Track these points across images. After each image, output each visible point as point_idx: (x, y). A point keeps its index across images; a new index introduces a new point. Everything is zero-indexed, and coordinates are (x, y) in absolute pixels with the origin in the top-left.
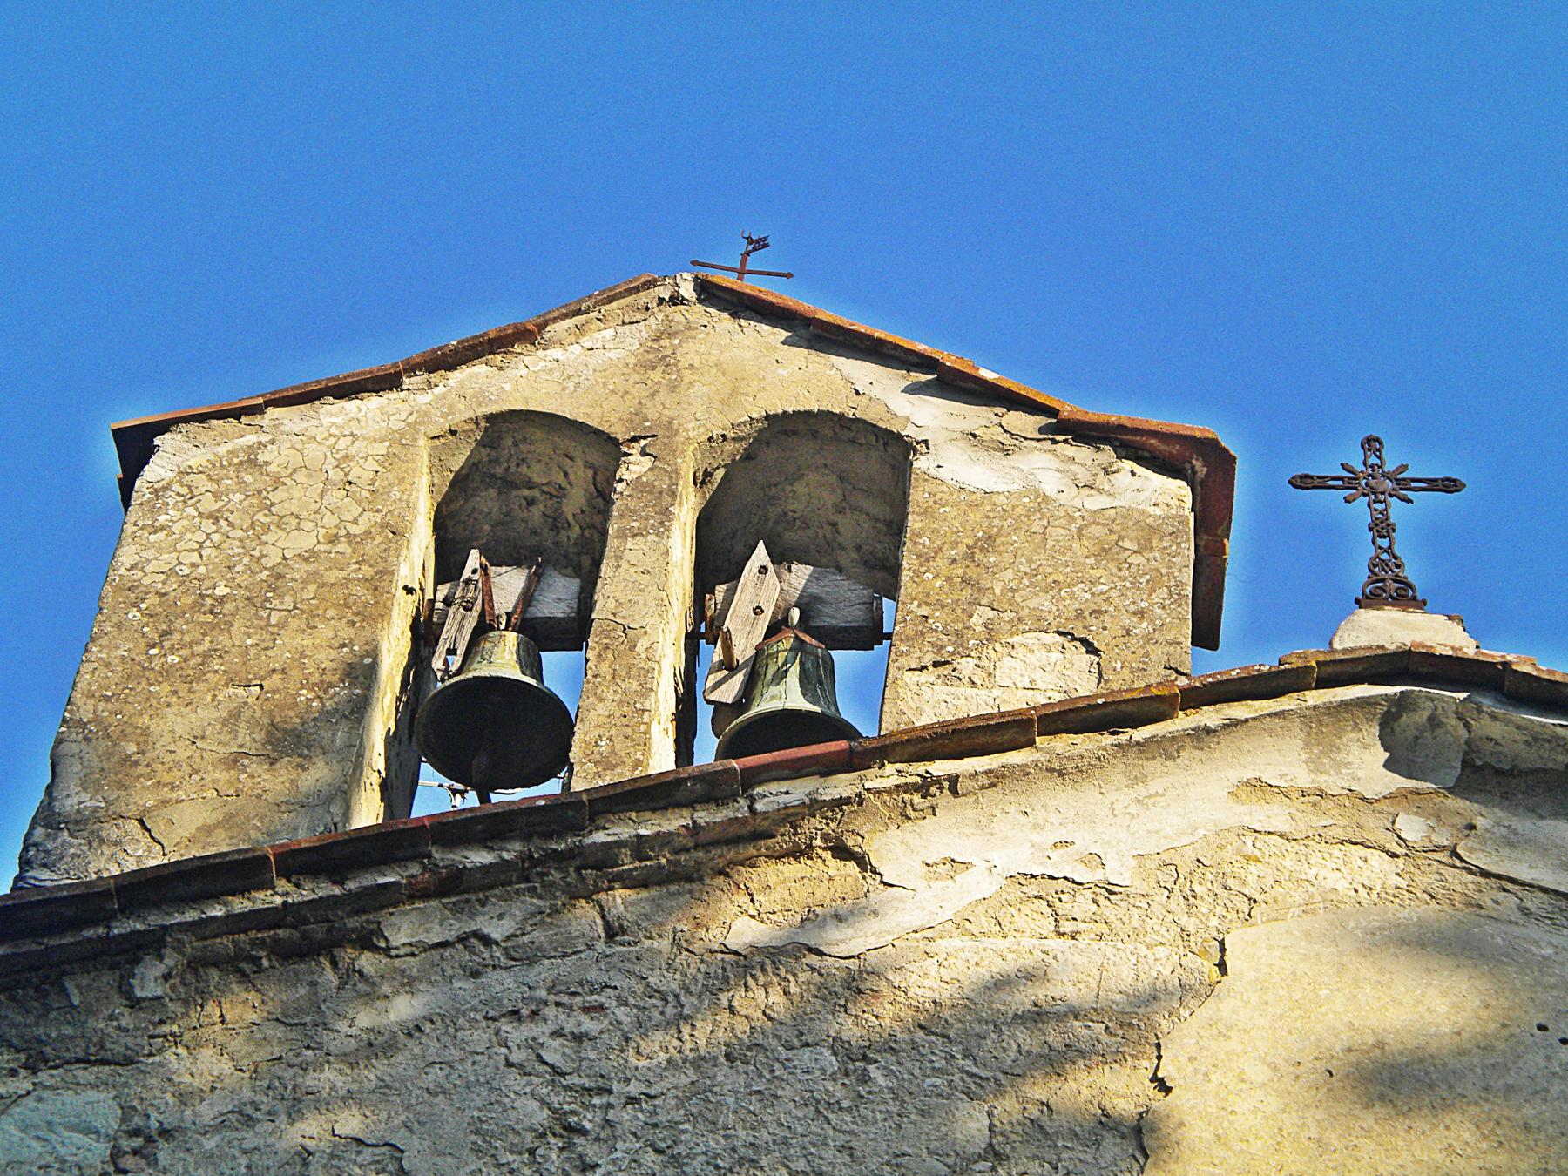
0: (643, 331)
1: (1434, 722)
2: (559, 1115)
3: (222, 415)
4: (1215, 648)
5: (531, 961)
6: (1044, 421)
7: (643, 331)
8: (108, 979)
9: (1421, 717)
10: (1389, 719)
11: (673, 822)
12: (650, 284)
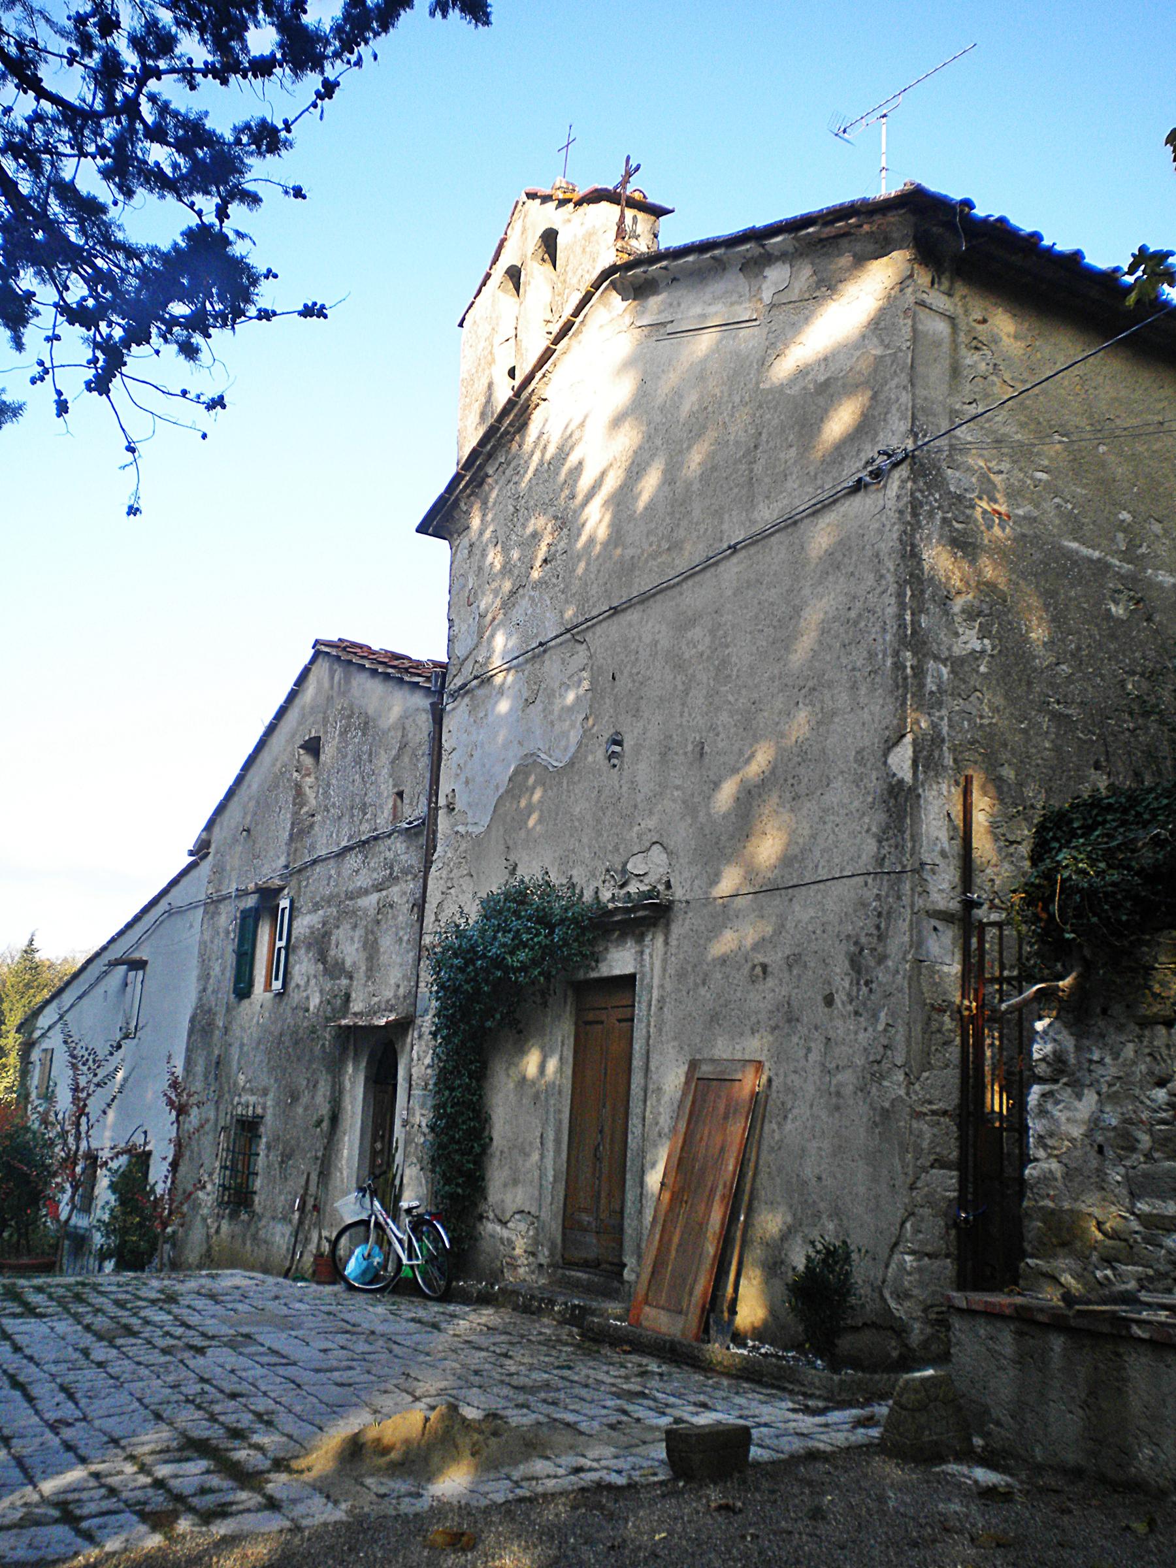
6: (571, 205)
10: (613, 285)
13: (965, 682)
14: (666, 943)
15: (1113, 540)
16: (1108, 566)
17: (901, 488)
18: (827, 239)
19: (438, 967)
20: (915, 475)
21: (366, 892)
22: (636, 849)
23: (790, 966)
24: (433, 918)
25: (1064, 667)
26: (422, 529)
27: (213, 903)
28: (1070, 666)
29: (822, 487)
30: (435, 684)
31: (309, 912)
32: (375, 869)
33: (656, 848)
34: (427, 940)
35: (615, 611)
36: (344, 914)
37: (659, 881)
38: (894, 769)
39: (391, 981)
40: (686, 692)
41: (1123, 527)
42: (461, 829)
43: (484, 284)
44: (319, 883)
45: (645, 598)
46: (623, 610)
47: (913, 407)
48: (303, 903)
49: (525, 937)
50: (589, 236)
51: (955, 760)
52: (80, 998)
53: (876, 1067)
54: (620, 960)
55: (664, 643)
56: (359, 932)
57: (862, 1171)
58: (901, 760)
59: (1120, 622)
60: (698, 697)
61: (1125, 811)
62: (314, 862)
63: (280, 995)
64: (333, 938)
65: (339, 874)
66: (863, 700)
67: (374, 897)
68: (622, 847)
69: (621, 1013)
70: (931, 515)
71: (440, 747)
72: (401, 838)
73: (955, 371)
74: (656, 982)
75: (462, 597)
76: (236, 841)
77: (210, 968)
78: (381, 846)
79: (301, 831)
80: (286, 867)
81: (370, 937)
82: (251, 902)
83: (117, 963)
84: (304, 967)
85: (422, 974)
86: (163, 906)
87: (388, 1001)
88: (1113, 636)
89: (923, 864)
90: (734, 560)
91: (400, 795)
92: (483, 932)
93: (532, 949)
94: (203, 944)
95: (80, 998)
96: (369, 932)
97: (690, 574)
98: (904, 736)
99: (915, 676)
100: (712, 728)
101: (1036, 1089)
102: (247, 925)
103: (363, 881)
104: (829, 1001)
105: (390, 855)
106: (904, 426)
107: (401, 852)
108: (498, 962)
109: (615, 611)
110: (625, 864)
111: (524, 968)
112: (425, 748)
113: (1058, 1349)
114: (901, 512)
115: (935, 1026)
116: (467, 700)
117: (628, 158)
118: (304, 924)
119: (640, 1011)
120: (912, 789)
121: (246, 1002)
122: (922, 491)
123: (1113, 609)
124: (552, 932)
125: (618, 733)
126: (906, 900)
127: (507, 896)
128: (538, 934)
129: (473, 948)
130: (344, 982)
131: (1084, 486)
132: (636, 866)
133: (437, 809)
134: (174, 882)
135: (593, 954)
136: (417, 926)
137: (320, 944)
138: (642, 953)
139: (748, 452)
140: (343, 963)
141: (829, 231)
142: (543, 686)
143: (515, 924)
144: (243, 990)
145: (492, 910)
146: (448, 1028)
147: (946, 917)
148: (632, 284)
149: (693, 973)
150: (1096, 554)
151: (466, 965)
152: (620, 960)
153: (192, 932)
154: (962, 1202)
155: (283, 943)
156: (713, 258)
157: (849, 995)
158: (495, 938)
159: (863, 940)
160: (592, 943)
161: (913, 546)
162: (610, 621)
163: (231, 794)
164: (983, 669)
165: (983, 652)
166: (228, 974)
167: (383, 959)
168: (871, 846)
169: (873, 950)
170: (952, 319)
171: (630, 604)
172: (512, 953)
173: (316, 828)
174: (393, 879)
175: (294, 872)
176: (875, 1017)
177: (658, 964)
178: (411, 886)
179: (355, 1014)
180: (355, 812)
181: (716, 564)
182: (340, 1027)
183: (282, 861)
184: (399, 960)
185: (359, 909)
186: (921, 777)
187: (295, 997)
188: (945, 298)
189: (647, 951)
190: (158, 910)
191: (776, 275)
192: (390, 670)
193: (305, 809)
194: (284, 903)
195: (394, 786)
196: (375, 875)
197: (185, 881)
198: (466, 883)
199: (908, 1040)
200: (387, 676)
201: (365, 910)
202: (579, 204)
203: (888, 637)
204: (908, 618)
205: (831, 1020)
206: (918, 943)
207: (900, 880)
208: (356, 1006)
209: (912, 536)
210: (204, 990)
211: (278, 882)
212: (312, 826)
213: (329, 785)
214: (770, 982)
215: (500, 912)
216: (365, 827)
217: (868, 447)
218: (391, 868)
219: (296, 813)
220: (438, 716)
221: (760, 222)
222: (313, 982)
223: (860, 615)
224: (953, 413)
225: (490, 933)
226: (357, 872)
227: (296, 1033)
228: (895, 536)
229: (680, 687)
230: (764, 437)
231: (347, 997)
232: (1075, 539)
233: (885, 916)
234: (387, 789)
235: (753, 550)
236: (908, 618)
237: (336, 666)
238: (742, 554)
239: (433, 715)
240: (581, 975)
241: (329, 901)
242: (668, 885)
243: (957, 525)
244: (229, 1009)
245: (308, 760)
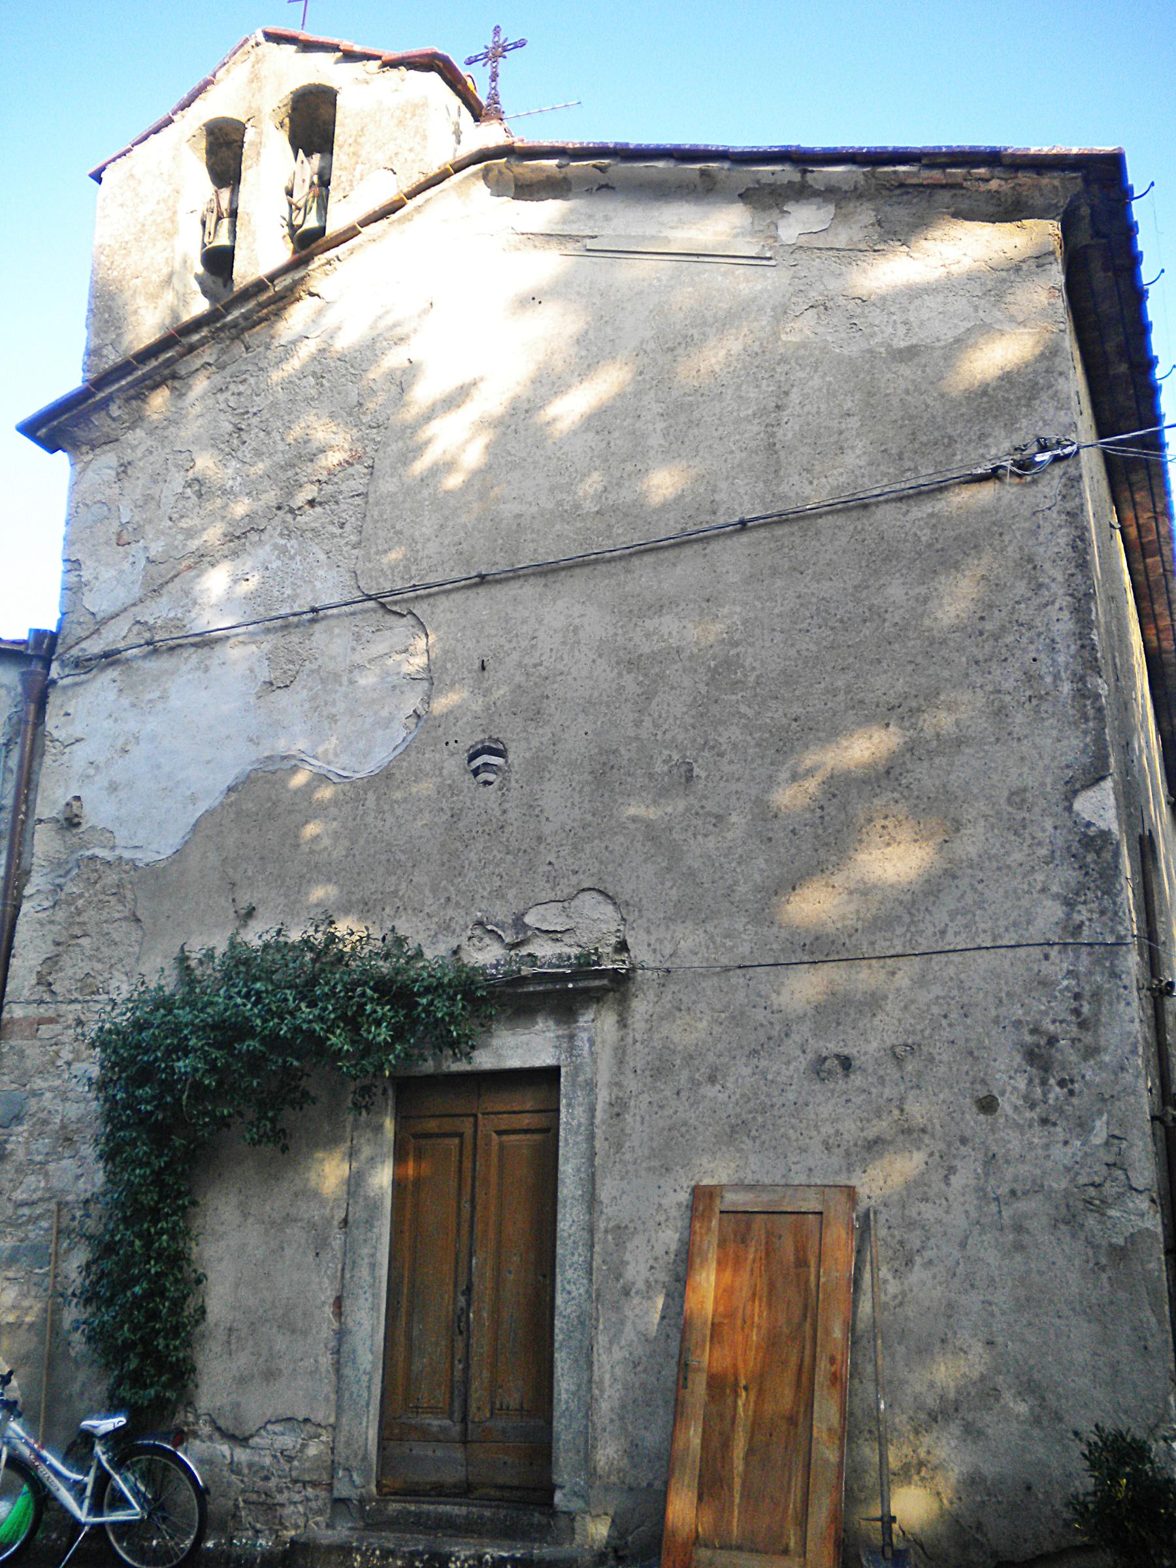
0: (248, 64)
1: (500, 172)
2: (235, 425)
3: (119, 156)
4: (1113, 164)
5: (224, 368)
6: (379, 62)
7: (248, 64)
8: (103, 413)
9: (496, 172)
10: (485, 175)
11: (252, 304)
12: (247, 40)
14: (623, 1023)
18: (911, 185)
26: (30, 429)
43: (156, 131)
53: (1092, 1192)
57: (1081, 1331)
74: (603, 1077)
90: (744, 538)
98: (1103, 778)
104: (987, 1105)
138: (571, 1037)
148: (516, 179)
156: (703, 173)
157: (1026, 1098)
162: (471, 593)
176: (1083, 1126)
205: (993, 1131)
214: (857, 1080)
223: (1003, 628)
242: (622, 947)
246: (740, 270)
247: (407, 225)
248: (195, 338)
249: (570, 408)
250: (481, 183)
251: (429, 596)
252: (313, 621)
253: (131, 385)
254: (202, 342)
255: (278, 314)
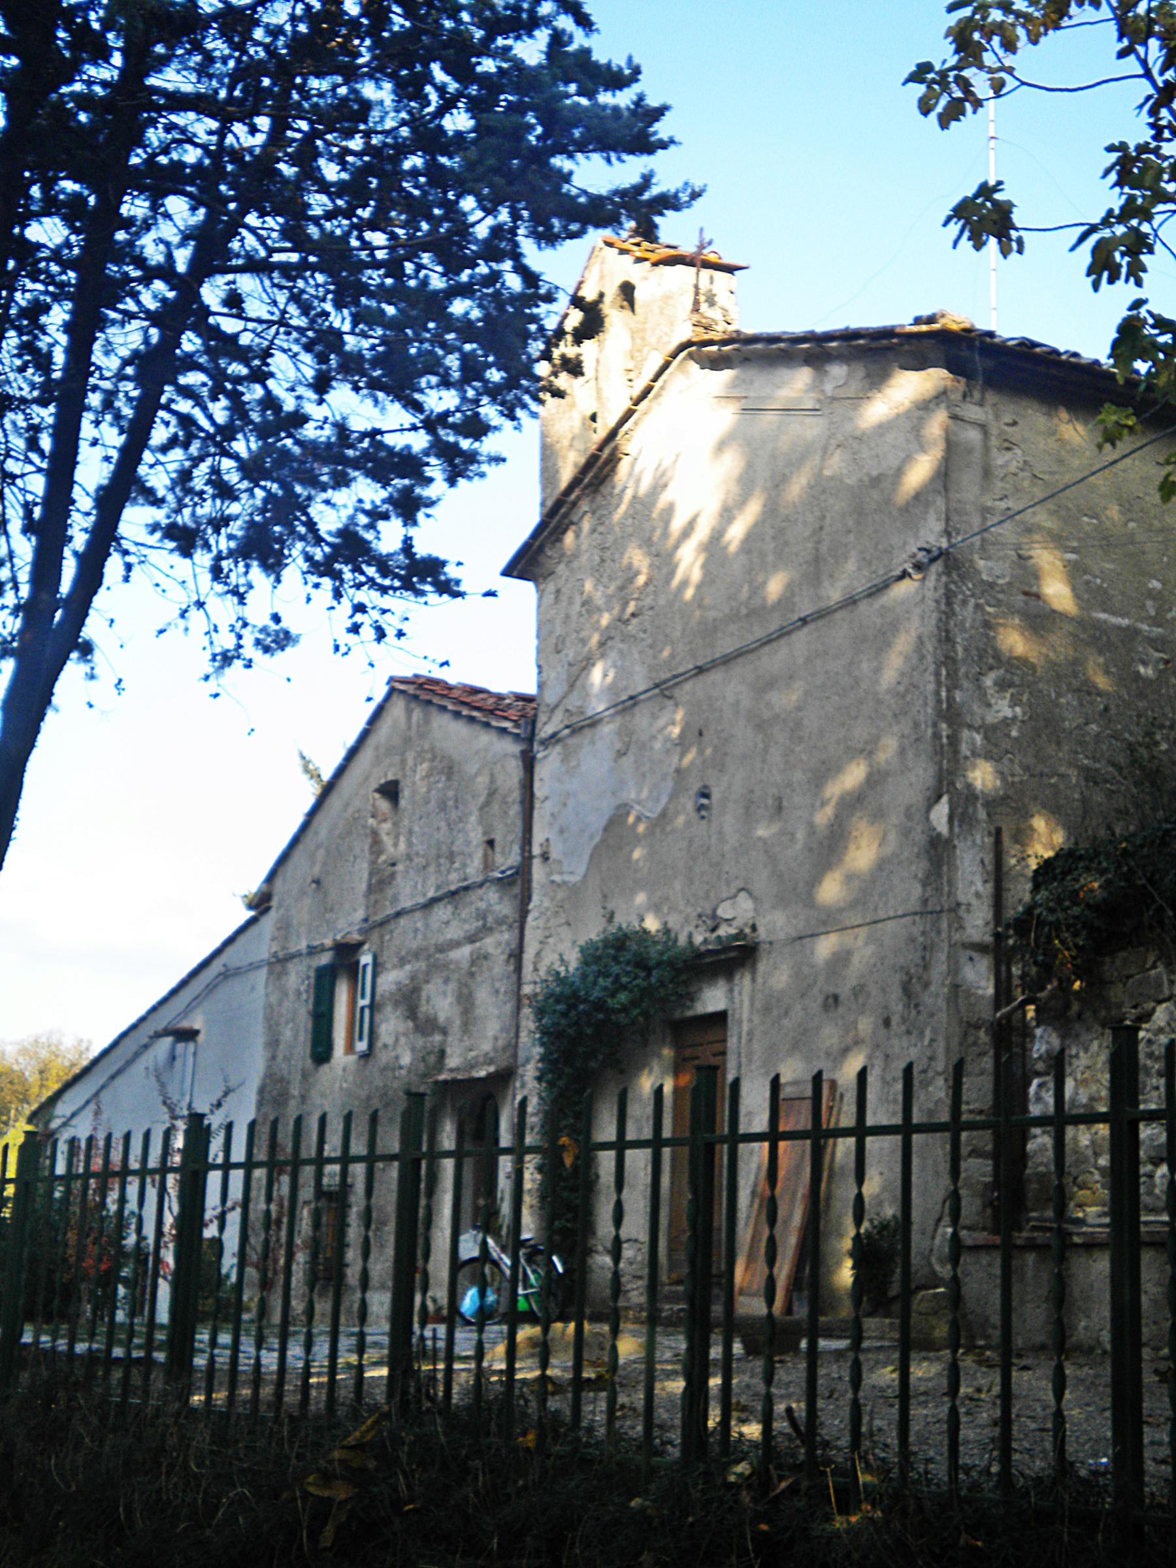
6: (647, 264)
10: (691, 356)
11: (594, 470)
13: (996, 745)
14: (753, 980)
15: (1143, 607)
16: (1137, 632)
17: (938, 580)
18: (877, 350)
19: (540, 1013)
20: (948, 571)
21: (457, 944)
22: (724, 895)
23: (856, 996)
24: (531, 968)
25: (1094, 726)
26: (507, 572)
27: (280, 963)
28: (1099, 725)
29: (875, 572)
30: (516, 719)
31: (395, 967)
32: (465, 921)
33: (743, 894)
34: (527, 989)
35: (700, 670)
36: (435, 967)
37: (746, 924)
38: (935, 823)
39: (488, 1032)
40: (766, 750)
41: (1151, 594)
42: (557, 878)
44: (406, 935)
45: (727, 660)
46: (708, 670)
47: (948, 509)
48: (388, 957)
49: (624, 980)
50: (667, 298)
51: (989, 815)
52: (113, 1077)
54: (713, 999)
55: (746, 702)
56: (452, 986)
58: (940, 813)
59: (1147, 681)
60: (775, 755)
61: (1091, 860)
62: (398, 914)
63: (366, 1056)
64: (424, 994)
65: (427, 926)
66: (910, 764)
67: (466, 951)
68: (712, 895)
69: (717, 1047)
70: (964, 602)
71: (532, 795)
72: (494, 888)
73: (987, 473)
75: (551, 642)
76: (303, 893)
77: (280, 1033)
78: (473, 896)
79: (381, 882)
80: (366, 920)
81: (465, 991)
82: (325, 959)
83: (166, 1032)
84: (391, 1025)
85: (523, 1023)
86: (216, 967)
87: (486, 1054)
88: (1141, 695)
89: (958, 905)
90: (805, 630)
91: (491, 843)
92: (584, 976)
93: (631, 991)
94: (269, 1007)
95: (113, 1077)
96: (462, 985)
97: (768, 641)
99: (950, 744)
100: (789, 785)
101: (1035, 1082)
102: (324, 983)
103: (454, 932)
104: (887, 1023)
105: (482, 905)
106: (939, 527)
107: (497, 903)
108: (600, 1005)
109: (700, 670)
110: (715, 910)
111: (624, 1009)
112: (516, 795)
113: (1030, 1263)
114: (937, 602)
115: (971, 1039)
116: (558, 748)
117: (701, 230)
118: (390, 980)
119: (732, 1042)
120: (949, 841)
121: (325, 1068)
122: (955, 583)
123: (1142, 670)
124: (649, 975)
125: (705, 787)
126: (944, 935)
127: (606, 943)
128: (636, 977)
129: (575, 994)
130: (438, 1038)
131: (1113, 561)
132: (724, 911)
133: (531, 857)
134: (230, 941)
135: (688, 994)
136: (514, 977)
137: (409, 1000)
139: (814, 532)
140: (435, 1019)
141: (874, 345)
142: (634, 738)
143: (616, 969)
144: (321, 1052)
145: (592, 956)
146: (551, 1071)
147: (981, 948)
149: (770, 1007)
150: (1125, 622)
151: (569, 1009)
152: (713, 999)
153: (256, 991)
154: (996, 1184)
155: (366, 1002)
158: (595, 983)
159: (912, 971)
160: (687, 983)
161: (947, 631)
162: (694, 680)
163: (296, 841)
164: (1014, 733)
165: (1014, 718)
166: (301, 1038)
167: (479, 1012)
168: (917, 890)
169: (919, 978)
170: (983, 428)
171: (714, 665)
172: (613, 995)
173: (399, 878)
174: (486, 930)
175: (375, 926)
176: (922, 1034)
177: (746, 1003)
178: (506, 936)
179: (451, 1070)
180: (442, 861)
181: (789, 633)
182: (436, 1082)
183: (360, 914)
184: (496, 1012)
185: (451, 962)
186: (956, 830)
187: (383, 1057)
188: (977, 408)
189: (737, 989)
190: (211, 974)
191: (838, 371)
192: (475, 714)
193: (383, 858)
194: (366, 959)
195: (484, 834)
196: (467, 927)
197: (242, 940)
198: (565, 932)
199: (948, 1050)
200: (472, 719)
201: (457, 962)
202: (655, 264)
203: (929, 710)
204: (944, 694)
206: (954, 969)
207: (938, 920)
208: (453, 1061)
209: (947, 623)
210: (274, 1058)
211: (356, 937)
212: (393, 876)
213: (411, 832)
215: (599, 958)
216: (454, 876)
217: (912, 541)
218: (485, 918)
219: (373, 863)
220: (529, 763)
221: (820, 328)
222: (403, 1040)
224: (985, 511)
225: (591, 978)
226: (447, 923)
227: (385, 1094)
228: (933, 622)
229: (761, 745)
230: (828, 521)
231: (442, 1054)
232: (1105, 611)
233: (928, 948)
234: (476, 836)
235: (820, 623)
236: (944, 694)
237: (413, 705)
238: (812, 626)
239: (524, 761)
240: (677, 1015)
241: (416, 955)
242: (754, 928)
243: (989, 609)
244: (305, 1076)
245: (384, 805)
246: (808, 420)
247: (661, 400)
248: (573, 497)
249: (736, 532)
250: (692, 363)
251: (677, 684)
252: (635, 704)
253: (551, 534)
254: (579, 498)
255: (613, 470)
